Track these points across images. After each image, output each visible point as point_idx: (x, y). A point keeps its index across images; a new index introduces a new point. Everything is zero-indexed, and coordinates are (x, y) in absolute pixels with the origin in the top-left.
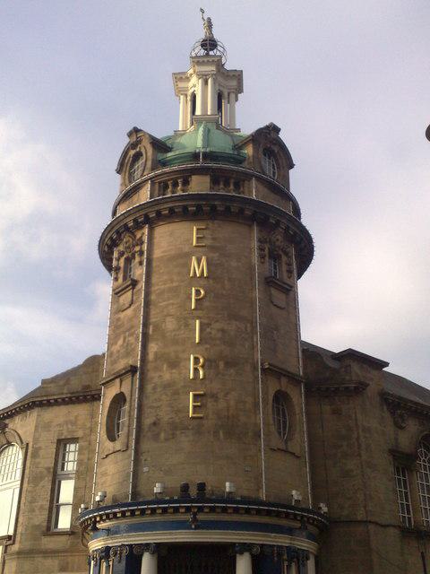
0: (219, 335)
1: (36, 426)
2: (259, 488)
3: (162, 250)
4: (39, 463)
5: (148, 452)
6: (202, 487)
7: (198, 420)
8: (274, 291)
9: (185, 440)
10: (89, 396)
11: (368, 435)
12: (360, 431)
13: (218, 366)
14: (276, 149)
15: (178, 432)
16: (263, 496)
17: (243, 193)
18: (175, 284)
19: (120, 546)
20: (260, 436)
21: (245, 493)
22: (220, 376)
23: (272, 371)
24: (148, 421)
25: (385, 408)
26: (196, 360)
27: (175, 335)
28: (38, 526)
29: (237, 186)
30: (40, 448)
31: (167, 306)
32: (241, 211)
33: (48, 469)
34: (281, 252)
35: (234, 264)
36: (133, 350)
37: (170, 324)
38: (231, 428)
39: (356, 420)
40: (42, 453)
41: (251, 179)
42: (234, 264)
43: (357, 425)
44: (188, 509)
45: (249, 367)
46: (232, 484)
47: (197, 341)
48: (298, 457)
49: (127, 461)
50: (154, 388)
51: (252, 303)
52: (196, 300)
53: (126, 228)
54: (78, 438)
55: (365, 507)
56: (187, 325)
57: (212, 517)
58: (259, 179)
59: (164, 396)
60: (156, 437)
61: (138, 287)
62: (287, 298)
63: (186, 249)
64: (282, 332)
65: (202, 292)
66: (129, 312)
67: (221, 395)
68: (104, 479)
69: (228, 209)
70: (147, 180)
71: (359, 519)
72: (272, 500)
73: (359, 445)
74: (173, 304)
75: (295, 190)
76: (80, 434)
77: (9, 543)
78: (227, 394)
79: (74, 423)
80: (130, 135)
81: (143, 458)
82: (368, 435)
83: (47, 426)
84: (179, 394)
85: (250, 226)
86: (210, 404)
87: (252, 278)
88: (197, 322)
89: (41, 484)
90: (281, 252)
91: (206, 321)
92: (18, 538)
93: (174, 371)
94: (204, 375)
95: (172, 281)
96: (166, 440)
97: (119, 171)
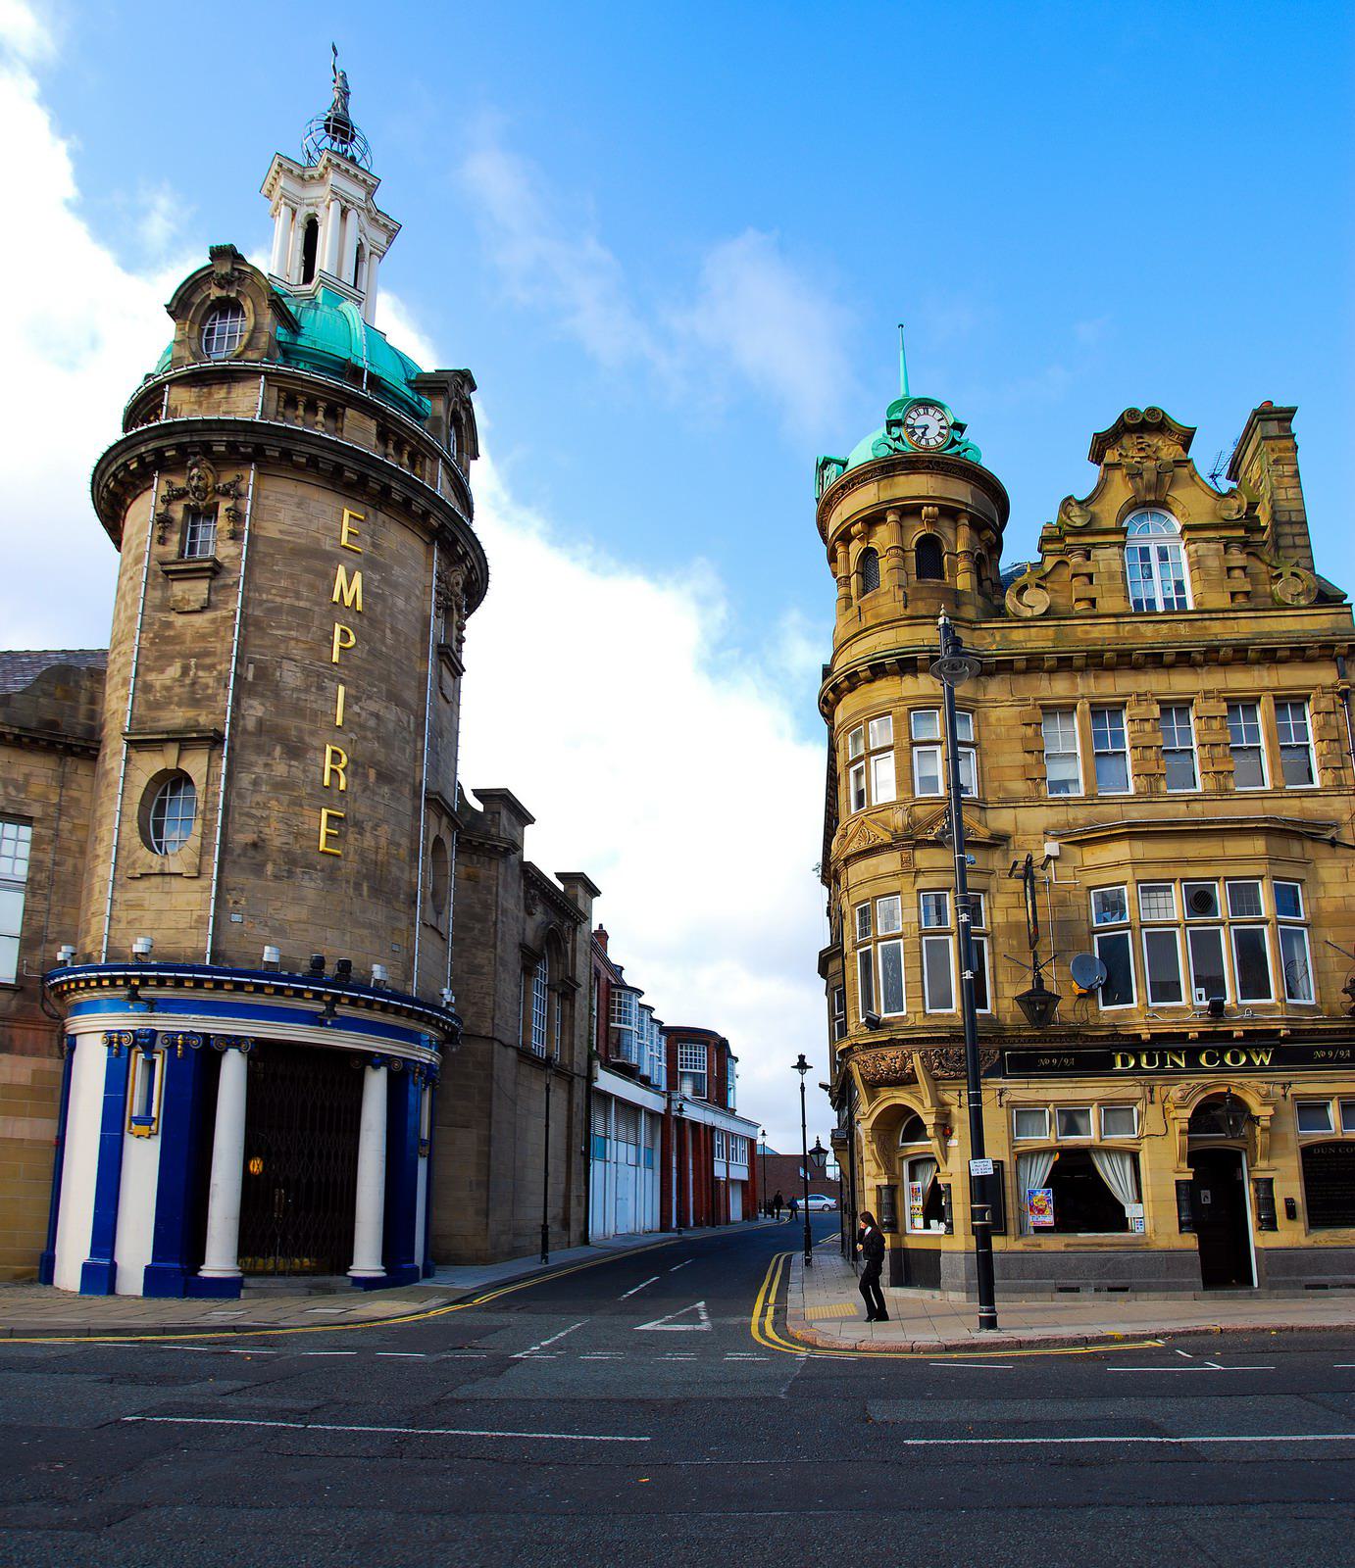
0: (372, 723)
2: (408, 977)
5: (242, 890)
6: (345, 966)
9: (310, 887)
13: (366, 776)
15: (298, 870)
18: (302, 604)
26: (336, 755)
27: (298, 699)
29: (412, 457)
31: (286, 639)
32: (426, 514)
35: (400, 603)
36: (212, 698)
37: (290, 676)
38: (378, 882)
39: (497, 896)
46: (384, 969)
47: (339, 722)
50: (255, 783)
51: (422, 681)
53: (206, 449)
56: (321, 688)
59: (273, 803)
60: (258, 869)
63: (327, 545)
64: (446, 740)
66: (200, 621)
67: (368, 826)
68: (133, 914)
69: (407, 502)
71: (484, 1034)
73: (496, 931)
74: (297, 640)
76: (35, 811)
79: (22, 787)
81: (230, 898)
84: (301, 806)
88: (341, 689)
91: (353, 692)
93: (293, 763)
96: (277, 877)
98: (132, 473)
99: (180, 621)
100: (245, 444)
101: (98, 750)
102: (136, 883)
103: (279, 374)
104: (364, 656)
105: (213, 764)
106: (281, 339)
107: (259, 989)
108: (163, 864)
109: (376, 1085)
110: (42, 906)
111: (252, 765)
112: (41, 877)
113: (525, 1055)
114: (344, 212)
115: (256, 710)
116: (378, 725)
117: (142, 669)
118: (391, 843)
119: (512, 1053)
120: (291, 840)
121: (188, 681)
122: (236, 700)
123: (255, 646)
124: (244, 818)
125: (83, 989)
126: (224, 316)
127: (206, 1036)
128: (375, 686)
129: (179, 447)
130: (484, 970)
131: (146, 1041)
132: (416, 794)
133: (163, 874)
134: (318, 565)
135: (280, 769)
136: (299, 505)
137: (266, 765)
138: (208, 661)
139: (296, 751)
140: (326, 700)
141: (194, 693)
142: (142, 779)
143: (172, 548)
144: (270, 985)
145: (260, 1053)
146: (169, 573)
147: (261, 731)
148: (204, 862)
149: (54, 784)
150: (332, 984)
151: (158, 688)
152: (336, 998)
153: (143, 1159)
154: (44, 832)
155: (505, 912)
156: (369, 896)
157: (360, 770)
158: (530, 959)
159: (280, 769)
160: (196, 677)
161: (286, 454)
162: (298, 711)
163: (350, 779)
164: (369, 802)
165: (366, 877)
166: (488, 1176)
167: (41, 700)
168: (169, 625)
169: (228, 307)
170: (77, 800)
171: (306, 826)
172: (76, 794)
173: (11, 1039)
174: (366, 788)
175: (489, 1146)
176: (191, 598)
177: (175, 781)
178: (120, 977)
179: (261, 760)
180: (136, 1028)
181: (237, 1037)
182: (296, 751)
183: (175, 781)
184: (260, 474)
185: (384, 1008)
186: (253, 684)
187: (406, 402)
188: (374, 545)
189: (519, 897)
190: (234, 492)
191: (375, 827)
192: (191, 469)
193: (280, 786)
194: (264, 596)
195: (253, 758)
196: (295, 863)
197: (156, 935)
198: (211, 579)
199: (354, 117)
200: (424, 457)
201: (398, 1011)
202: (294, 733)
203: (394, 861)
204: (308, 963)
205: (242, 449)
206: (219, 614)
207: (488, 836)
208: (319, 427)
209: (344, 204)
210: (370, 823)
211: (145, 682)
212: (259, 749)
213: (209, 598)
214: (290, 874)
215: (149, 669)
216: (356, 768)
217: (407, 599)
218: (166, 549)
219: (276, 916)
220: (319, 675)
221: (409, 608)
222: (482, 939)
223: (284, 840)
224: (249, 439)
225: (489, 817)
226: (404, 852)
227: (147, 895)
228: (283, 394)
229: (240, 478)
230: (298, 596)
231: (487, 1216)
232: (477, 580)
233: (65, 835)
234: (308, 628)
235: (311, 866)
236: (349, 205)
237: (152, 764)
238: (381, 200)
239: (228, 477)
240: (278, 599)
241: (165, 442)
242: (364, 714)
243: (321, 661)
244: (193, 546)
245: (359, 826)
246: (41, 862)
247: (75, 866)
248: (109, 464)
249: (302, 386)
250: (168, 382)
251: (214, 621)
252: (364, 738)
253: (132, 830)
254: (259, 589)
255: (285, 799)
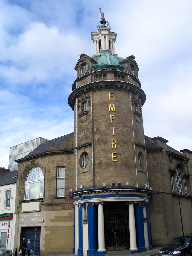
0: (121, 132)
1: (48, 162)
2: (135, 183)
3: (98, 100)
4: (51, 174)
7: (115, 162)
8: (137, 117)
9: (111, 169)
10: (69, 152)
11: (163, 165)
12: (161, 164)
13: (121, 144)
14: (134, 64)
15: (109, 166)
16: (137, 186)
17: (125, 80)
18: (103, 114)
19: (90, 203)
20: (135, 167)
21: (131, 185)
22: (122, 147)
23: (138, 145)
24: (97, 162)
25: (167, 155)
27: (105, 132)
28: (53, 195)
29: (123, 77)
30: (50, 169)
31: (101, 121)
33: (54, 176)
34: (137, 102)
35: (124, 107)
36: (89, 137)
37: (103, 128)
38: (126, 165)
39: (160, 160)
40: (51, 171)
41: (128, 75)
42: (124, 107)
43: (160, 162)
44: (115, 191)
45: (131, 143)
47: (113, 135)
48: (145, 173)
49: (90, 175)
50: (99, 151)
51: (131, 121)
52: (112, 120)
54: (64, 166)
55: (163, 188)
56: (109, 129)
57: (122, 193)
58: (130, 76)
59: (102, 154)
60: (101, 168)
61: (89, 114)
62: (140, 119)
63: (107, 101)
64: (140, 131)
65: (114, 117)
66: (86, 123)
67: (122, 154)
68: (80, 181)
70: (90, 74)
72: (139, 187)
73: (161, 168)
74: (103, 121)
75: (140, 78)
76: (65, 165)
77: (42, 201)
78: (124, 153)
79: (62, 161)
80: (81, 56)
81: (96, 174)
82: (163, 165)
83: (52, 162)
84: (108, 153)
85: (128, 93)
86: (119, 157)
87: (130, 112)
88: (113, 128)
89: (53, 181)
90: (137, 102)
92: (46, 199)
93: (105, 145)
94: (116, 147)
95: (103, 113)
96: (105, 168)
97: (76, 69)
98: (73, 100)
99: (82, 124)
100: (89, 88)
101: (74, 151)
102: (80, 175)
103: (94, 73)
104: (117, 120)
105: (90, 149)
106: (94, 66)
107: (103, 192)
108: (84, 170)
109: (131, 209)
110: (67, 182)
111: (97, 147)
112: (67, 176)
113: (176, 196)
114: (105, 37)
115: (97, 137)
116: (122, 133)
117: (78, 135)
118: (128, 156)
119: (170, 195)
120: (106, 160)
121: (85, 135)
122: (93, 136)
123: (96, 125)
124: (97, 158)
125: (75, 196)
126: (84, 66)
127: (94, 202)
128: (120, 125)
129: (79, 93)
130: (159, 178)
131: (84, 205)
132: (133, 144)
133: (84, 172)
134: (106, 105)
135: (103, 147)
136: (101, 95)
137: (100, 147)
138: (88, 130)
139: (105, 143)
140: (110, 131)
141: (86, 137)
142: (79, 155)
143: (80, 110)
144: (105, 191)
145: (106, 205)
146: (80, 116)
147: (99, 141)
148: (91, 168)
149: (68, 159)
150: (118, 189)
151: (81, 137)
152: (119, 191)
153: (86, 228)
154: (67, 168)
155: (163, 163)
156: (124, 168)
157: (119, 143)
158: (172, 173)
159: (103, 147)
160: (86, 133)
161: (96, 87)
162: (105, 135)
163: (117, 145)
164: (122, 149)
165: (123, 164)
166: (166, 225)
167: (64, 144)
168: (81, 125)
169: (84, 64)
170: (72, 161)
171: (109, 157)
172: (71, 160)
173: (65, 207)
174: (121, 146)
175: (166, 218)
176: (84, 119)
177: (85, 154)
178: (81, 193)
179: (99, 146)
180: (82, 203)
181: (100, 202)
182: (105, 143)
183: (85, 154)
184: (93, 92)
185: (130, 191)
186: (96, 132)
187: (120, 67)
188: (117, 97)
189: (167, 159)
190: (89, 97)
191: (124, 153)
192: (81, 96)
193: (103, 150)
194: (96, 115)
195: (98, 146)
196: (108, 165)
197: (84, 184)
198: (87, 114)
199: (106, 19)
200: (125, 76)
201: (133, 191)
202: (105, 139)
203: (129, 160)
204: (112, 185)
205: (89, 89)
206: (89, 120)
207: (156, 148)
208: (102, 80)
209: (105, 35)
210: (123, 153)
211: (78, 137)
212: (99, 144)
213: (87, 118)
214: (107, 167)
215: (79, 134)
216: (118, 142)
217: (125, 105)
218: (79, 111)
219: (105, 176)
220: (108, 126)
221: (126, 107)
222: (158, 171)
223: (105, 161)
224: (89, 87)
225: (156, 143)
226: (131, 157)
227: (82, 177)
228: (95, 76)
229: (89, 94)
230: (103, 113)
231: (167, 235)
232: (142, 95)
233: (70, 168)
234: (105, 118)
235: (111, 165)
236: (105, 35)
237: (81, 151)
238: (112, 31)
239: (87, 95)
240: (99, 114)
241: (76, 93)
242: (119, 131)
243: (108, 123)
244: (84, 109)
245: (120, 154)
246: (67, 174)
247: (73, 174)
248: (70, 99)
249: (98, 73)
250: (76, 82)
251: (88, 122)
252: (119, 136)
253: (79, 165)
254: (95, 114)
255: (105, 153)
